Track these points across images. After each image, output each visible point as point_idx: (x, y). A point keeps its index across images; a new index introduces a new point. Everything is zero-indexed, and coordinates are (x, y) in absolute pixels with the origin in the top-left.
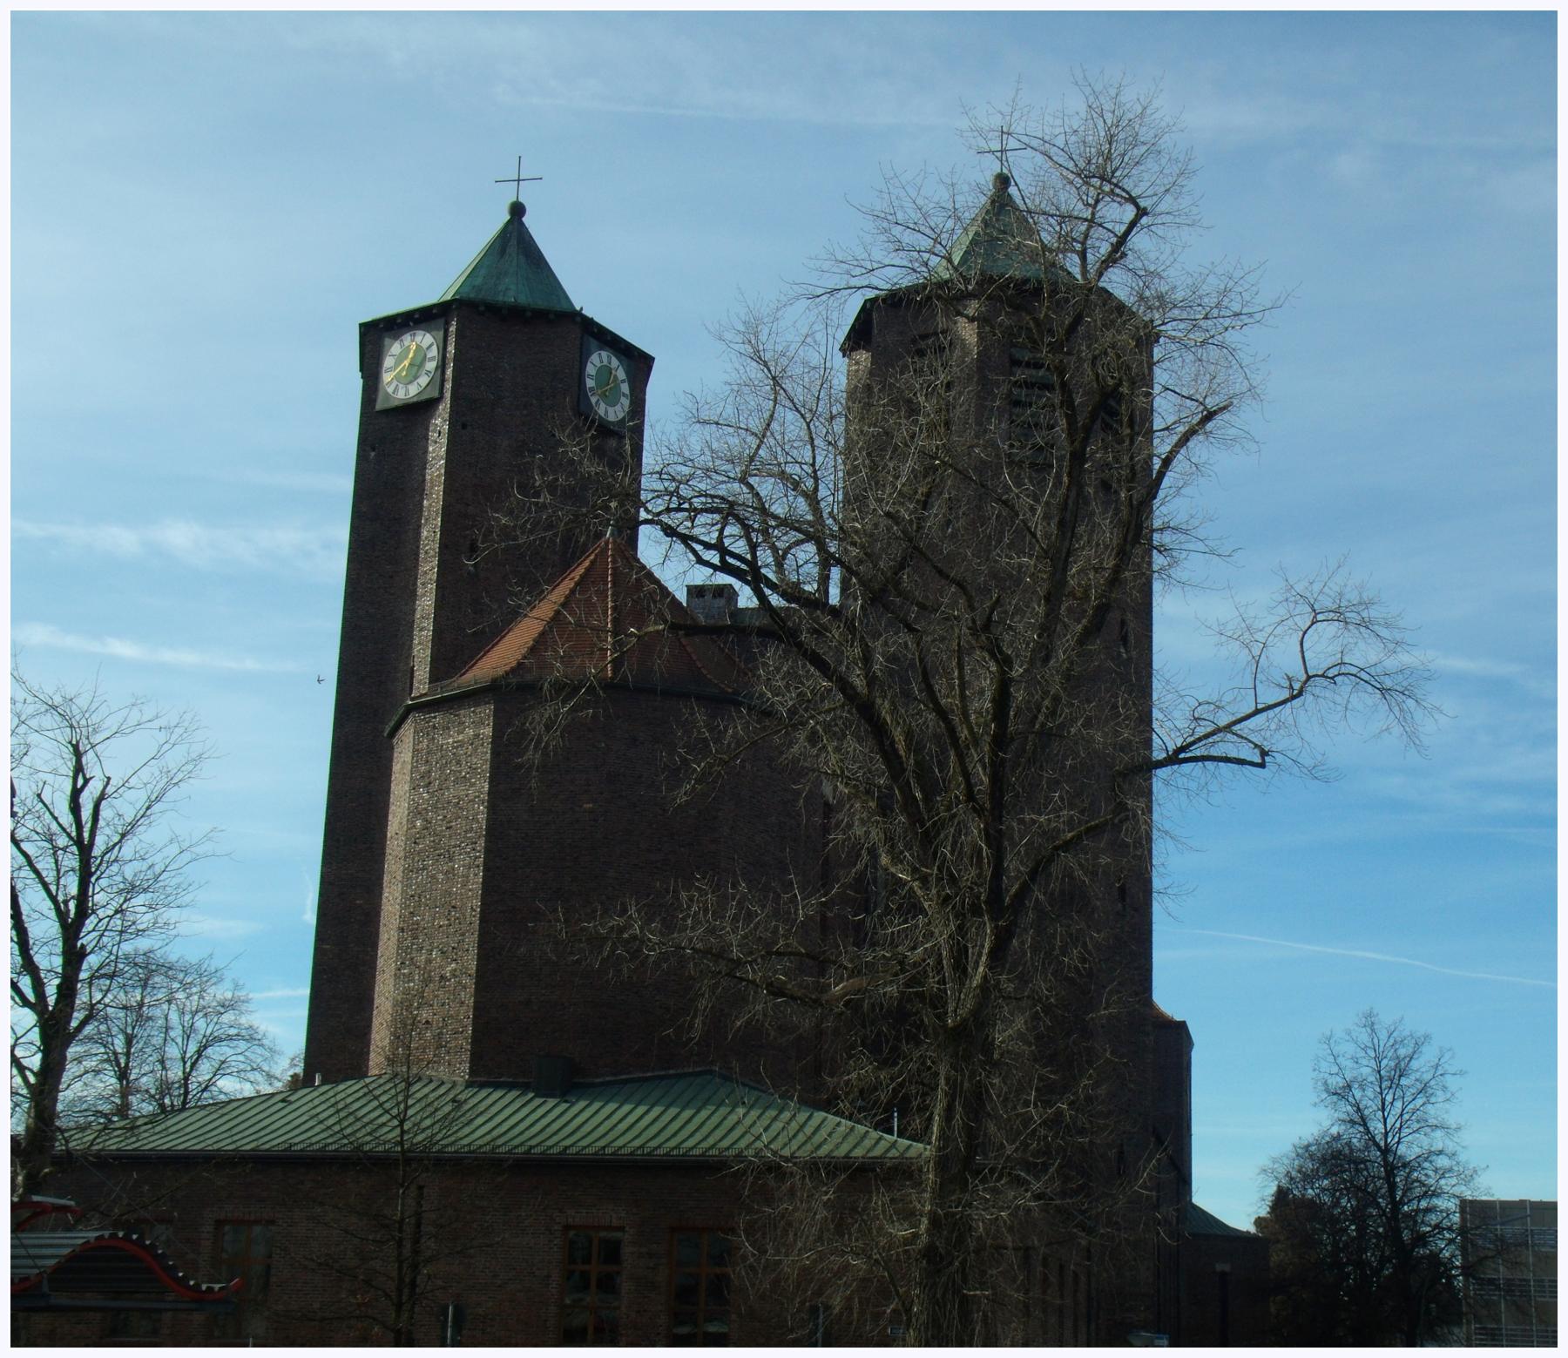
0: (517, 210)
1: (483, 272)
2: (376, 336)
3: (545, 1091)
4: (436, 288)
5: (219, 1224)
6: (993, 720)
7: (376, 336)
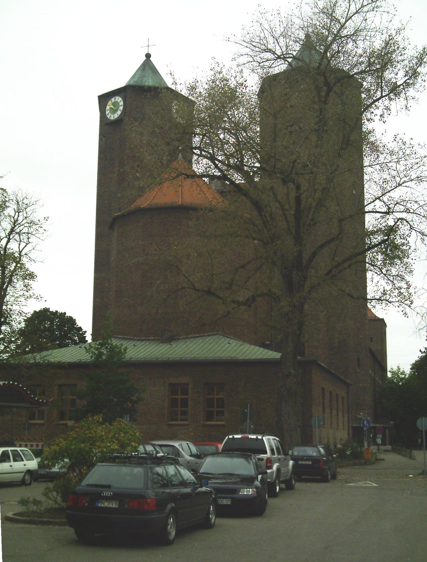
0: (148, 56)
1: (137, 76)
2: (104, 99)
3: (163, 342)
4: (122, 84)
5: (60, 386)
6: (25, 321)
7: (104, 99)
